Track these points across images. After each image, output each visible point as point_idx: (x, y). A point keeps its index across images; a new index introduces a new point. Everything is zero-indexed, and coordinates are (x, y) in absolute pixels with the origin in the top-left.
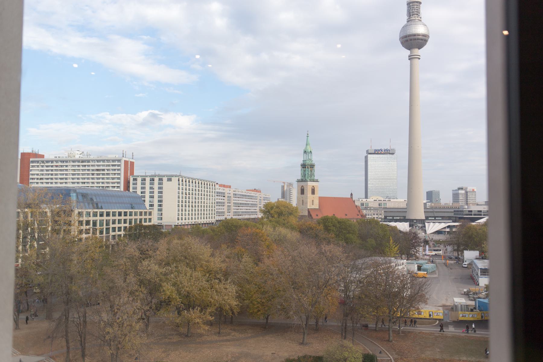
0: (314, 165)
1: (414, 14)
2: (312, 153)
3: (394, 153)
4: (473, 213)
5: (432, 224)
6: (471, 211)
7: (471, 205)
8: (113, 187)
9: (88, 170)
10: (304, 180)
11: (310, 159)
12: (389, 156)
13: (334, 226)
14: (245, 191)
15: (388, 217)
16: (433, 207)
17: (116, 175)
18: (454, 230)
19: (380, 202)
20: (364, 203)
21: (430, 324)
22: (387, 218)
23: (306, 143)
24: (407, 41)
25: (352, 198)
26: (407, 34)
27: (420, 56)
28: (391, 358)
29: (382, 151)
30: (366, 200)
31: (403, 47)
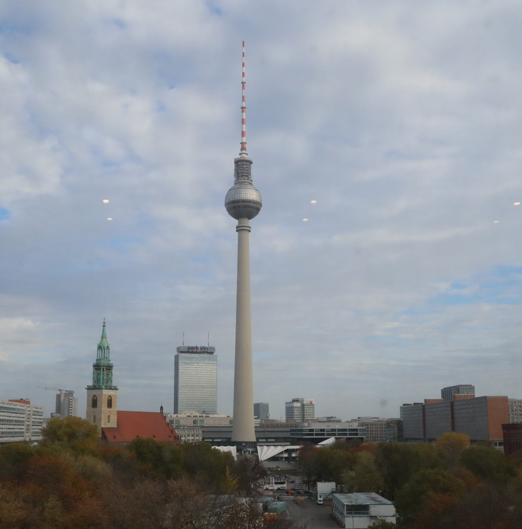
0: (112, 367)
2: (110, 349)
5: (265, 448)
6: (312, 430)
7: (310, 422)
10: (97, 387)
11: (106, 358)
12: (206, 355)
14: (8, 402)
15: (215, 439)
16: (264, 425)
18: (294, 455)
20: (173, 420)
23: (101, 335)
24: (234, 207)
29: (198, 350)
30: (177, 416)
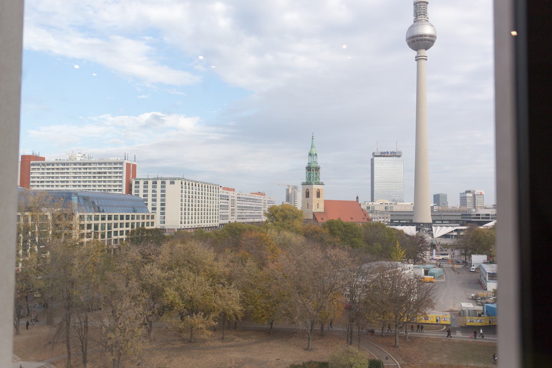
0: (320, 168)
1: (421, 14)
2: (318, 156)
3: (401, 156)
4: (481, 217)
5: (439, 228)
6: (479, 215)
7: (479, 208)
8: (115, 190)
9: (90, 173)
10: (309, 183)
11: (315, 162)
12: (395, 158)
13: (339, 229)
14: (249, 194)
15: (394, 221)
16: (440, 211)
17: (118, 177)
18: (461, 234)
19: (386, 205)
20: (370, 207)
21: (437, 329)
22: (394, 221)
23: (311, 145)
24: (414, 41)
25: (358, 202)
26: (414, 35)
27: (427, 57)
28: (398, 363)
29: (389, 154)
30: (373, 204)
31: (410, 47)
